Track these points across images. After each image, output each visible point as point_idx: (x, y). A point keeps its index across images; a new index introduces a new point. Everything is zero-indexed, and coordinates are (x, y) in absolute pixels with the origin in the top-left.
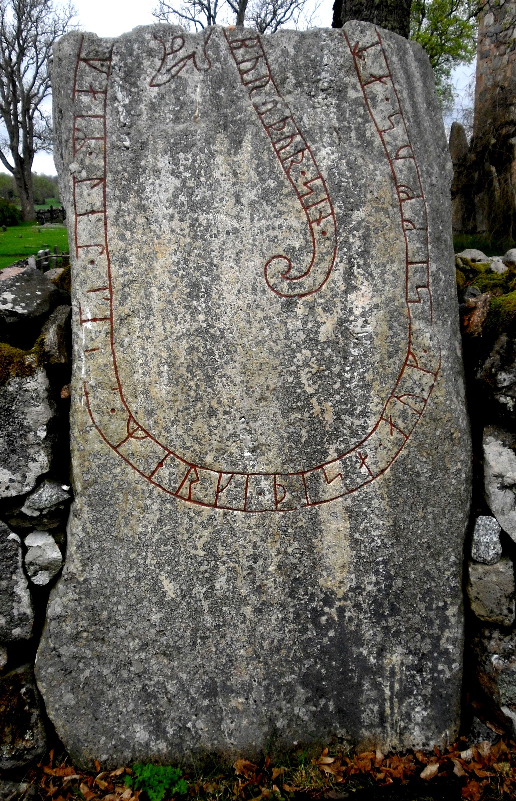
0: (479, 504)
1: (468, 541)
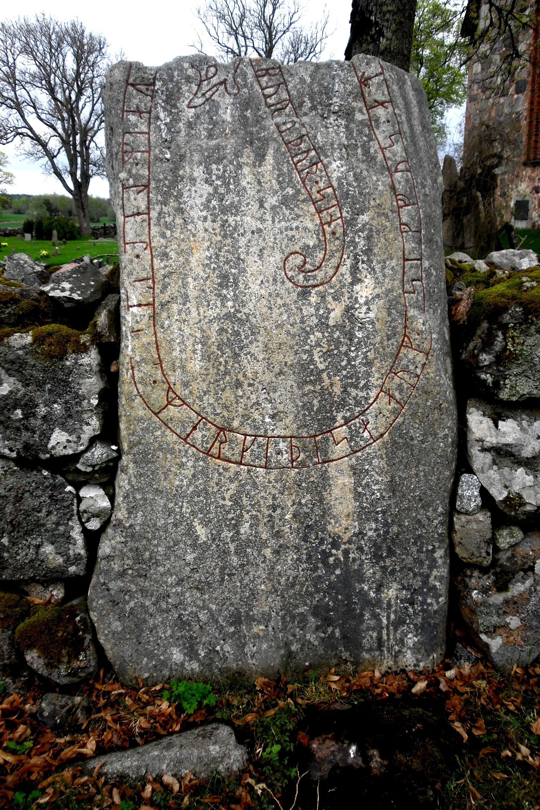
0: (463, 465)
1: (453, 495)
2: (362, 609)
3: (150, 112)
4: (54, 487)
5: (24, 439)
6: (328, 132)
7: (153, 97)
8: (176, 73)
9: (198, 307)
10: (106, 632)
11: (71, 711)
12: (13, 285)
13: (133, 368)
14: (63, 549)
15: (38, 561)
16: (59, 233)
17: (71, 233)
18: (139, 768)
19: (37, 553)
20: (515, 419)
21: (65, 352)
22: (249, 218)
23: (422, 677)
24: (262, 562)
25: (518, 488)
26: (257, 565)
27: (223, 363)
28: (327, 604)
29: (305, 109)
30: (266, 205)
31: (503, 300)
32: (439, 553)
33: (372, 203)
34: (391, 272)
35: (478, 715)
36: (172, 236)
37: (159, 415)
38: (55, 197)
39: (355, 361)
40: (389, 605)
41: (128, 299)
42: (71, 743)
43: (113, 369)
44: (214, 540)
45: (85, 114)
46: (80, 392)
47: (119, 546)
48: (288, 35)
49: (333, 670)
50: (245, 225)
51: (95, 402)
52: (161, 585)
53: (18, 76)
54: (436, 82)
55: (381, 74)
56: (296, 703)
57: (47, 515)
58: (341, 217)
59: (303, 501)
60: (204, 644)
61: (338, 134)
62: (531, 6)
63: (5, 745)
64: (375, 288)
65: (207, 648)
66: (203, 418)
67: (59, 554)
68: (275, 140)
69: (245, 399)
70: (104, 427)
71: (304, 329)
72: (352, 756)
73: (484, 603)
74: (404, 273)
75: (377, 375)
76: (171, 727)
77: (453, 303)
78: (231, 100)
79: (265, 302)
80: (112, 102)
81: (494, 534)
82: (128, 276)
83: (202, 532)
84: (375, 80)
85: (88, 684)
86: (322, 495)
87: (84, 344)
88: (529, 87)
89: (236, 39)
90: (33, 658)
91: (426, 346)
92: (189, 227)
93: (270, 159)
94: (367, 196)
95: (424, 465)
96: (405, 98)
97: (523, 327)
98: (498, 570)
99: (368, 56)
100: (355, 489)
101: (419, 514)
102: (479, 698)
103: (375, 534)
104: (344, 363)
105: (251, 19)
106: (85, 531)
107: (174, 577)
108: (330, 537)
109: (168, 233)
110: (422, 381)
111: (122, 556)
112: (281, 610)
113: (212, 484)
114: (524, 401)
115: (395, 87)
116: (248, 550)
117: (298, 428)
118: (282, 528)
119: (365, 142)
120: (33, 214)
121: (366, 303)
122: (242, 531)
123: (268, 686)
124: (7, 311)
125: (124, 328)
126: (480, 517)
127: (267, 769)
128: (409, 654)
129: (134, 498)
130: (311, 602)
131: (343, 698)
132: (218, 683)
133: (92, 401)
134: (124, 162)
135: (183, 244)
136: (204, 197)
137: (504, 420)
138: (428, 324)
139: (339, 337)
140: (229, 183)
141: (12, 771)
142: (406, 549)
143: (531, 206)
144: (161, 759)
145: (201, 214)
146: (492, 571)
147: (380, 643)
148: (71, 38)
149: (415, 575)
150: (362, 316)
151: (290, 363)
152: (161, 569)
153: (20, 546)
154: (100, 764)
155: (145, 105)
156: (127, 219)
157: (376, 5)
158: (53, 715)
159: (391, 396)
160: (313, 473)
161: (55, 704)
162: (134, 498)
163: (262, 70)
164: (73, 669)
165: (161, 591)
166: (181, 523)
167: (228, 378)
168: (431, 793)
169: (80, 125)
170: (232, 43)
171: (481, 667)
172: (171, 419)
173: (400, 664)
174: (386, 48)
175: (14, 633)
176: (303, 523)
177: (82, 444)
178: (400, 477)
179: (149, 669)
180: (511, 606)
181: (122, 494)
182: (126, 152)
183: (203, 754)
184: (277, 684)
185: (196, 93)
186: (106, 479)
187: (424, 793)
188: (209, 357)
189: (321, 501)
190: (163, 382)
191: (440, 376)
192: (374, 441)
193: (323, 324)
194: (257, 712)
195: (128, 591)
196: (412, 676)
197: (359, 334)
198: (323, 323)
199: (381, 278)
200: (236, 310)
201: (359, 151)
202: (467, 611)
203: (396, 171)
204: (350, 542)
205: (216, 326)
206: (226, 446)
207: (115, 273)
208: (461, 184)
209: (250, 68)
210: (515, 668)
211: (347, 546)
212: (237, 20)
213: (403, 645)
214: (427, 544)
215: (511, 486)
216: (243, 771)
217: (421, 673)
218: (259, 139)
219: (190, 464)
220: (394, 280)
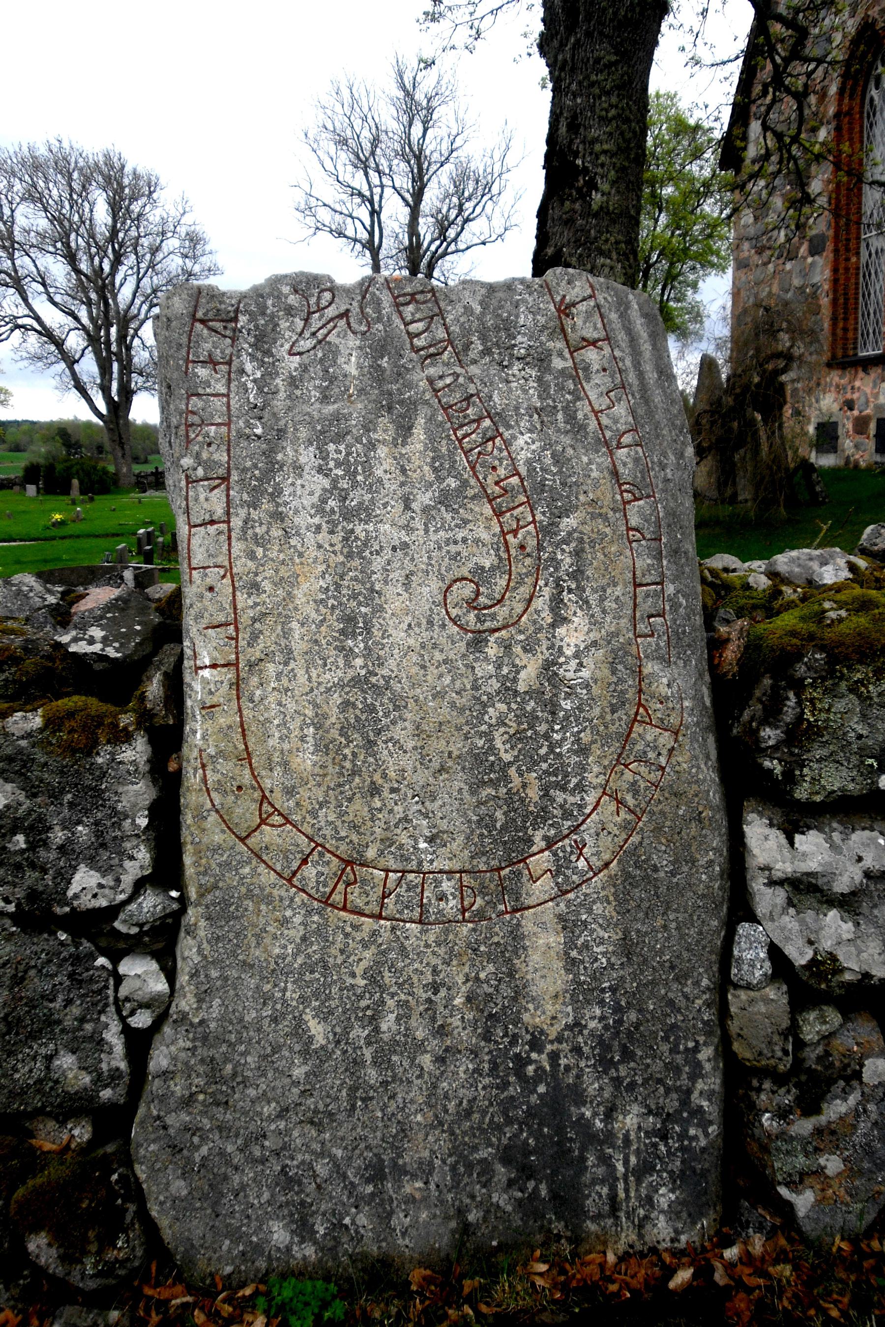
0: (740, 908)
1: (726, 957)
3: (229, 363)
4: (76, 959)
6: (510, 390)
7: (234, 339)
8: (270, 302)
9: (308, 668)
10: (162, 1198)
12: (13, 632)
13: (203, 766)
14: (90, 1061)
15: (49, 1081)
16: (81, 483)
19: (48, 1068)
20: (820, 830)
21: (96, 743)
22: (387, 526)
23: (685, 1260)
24: (418, 1077)
25: (829, 943)
26: (409, 1082)
27: (350, 757)
28: (525, 1142)
29: (473, 354)
30: (414, 506)
32: (706, 1054)
33: (582, 498)
34: (614, 606)
36: (265, 556)
37: (248, 841)
38: (75, 424)
39: (560, 747)
40: (627, 1141)
43: (172, 766)
44: (338, 1042)
45: (125, 294)
46: (120, 807)
47: (183, 1055)
49: (538, 1253)
50: (382, 538)
51: (143, 822)
52: (252, 1119)
53: (18, 236)
55: (590, 297)
57: (65, 1007)
58: (534, 521)
59: (482, 975)
60: (324, 1214)
61: (525, 392)
62: (828, 123)
65: (328, 1220)
66: (318, 845)
67: (85, 1069)
68: (427, 403)
69: (385, 812)
70: (156, 862)
71: (479, 699)
73: (782, 1135)
75: (596, 769)
77: (715, 645)
78: (358, 343)
79: (415, 658)
80: (170, 348)
82: (196, 619)
83: (318, 1030)
84: (582, 307)
86: (513, 965)
87: (125, 728)
88: (830, 246)
89: (366, 174)
91: (674, 720)
92: (293, 542)
93: (419, 433)
94: (574, 488)
95: (676, 911)
98: (803, 1078)
99: (570, 270)
100: (566, 953)
101: (670, 990)
102: (780, 1299)
103: (600, 1026)
104: (543, 751)
106: (127, 1031)
107: (273, 1105)
108: (527, 1032)
109: (260, 552)
110: (670, 775)
111: (188, 1071)
112: (450, 1155)
113: (334, 951)
114: (835, 800)
115: (614, 316)
116: (395, 1058)
117: (472, 857)
118: (449, 1020)
119: (568, 402)
120: (39, 452)
121: (576, 655)
122: (384, 1027)
125: (189, 703)
126: (771, 993)
128: (662, 1222)
130: (499, 1140)
131: (555, 1302)
132: (349, 1279)
133: (138, 821)
134: (189, 442)
135: (283, 569)
136: (317, 495)
137: (803, 833)
138: (676, 685)
139: (534, 710)
140: (355, 473)
142: (651, 1047)
143: (840, 431)
146: (795, 1080)
149: (668, 1091)
151: (456, 753)
152: (252, 1092)
153: (20, 1056)
155: (222, 352)
157: (583, 142)
159: (620, 802)
160: (497, 929)
163: (404, 295)
164: (106, 1263)
165: (252, 1127)
166: (283, 1015)
167: (357, 780)
169: (118, 312)
170: (359, 181)
171: (783, 1242)
172: (267, 848)
173: (647, 1238)
174: (601, 208)
176: (482, 1011)
178: (638, 931)
179: (233, 1260)
180: (827, 1138)
181: (187, 969)
182: (192, 425)
185: (302, 332)
186: (160, 945)
188: (326, 747)
189: (511, 974)
190: (253, 788)
191: (699, 768)
192: (595, 874)
193: (508, 690)
195: (198, 1129)
197: (567, 705)
198: (508, 689)
199: (599, 616)
201: (560, 416)
202: (755, 1147)
203: (618, 447)
204: (559, 1039)
205: (337, 698)
206: (356, 889)
208: (729, 401)
209: (386, 291)
210: (838, 1239)
211: (555, 1046)
212: (367, 146)
213: (652, 1206)
214: (686, 1039)
215: (819, 941)
217: (682, 1253)
218: (401, 402)
219: (298, 919)
220: (620, 617)
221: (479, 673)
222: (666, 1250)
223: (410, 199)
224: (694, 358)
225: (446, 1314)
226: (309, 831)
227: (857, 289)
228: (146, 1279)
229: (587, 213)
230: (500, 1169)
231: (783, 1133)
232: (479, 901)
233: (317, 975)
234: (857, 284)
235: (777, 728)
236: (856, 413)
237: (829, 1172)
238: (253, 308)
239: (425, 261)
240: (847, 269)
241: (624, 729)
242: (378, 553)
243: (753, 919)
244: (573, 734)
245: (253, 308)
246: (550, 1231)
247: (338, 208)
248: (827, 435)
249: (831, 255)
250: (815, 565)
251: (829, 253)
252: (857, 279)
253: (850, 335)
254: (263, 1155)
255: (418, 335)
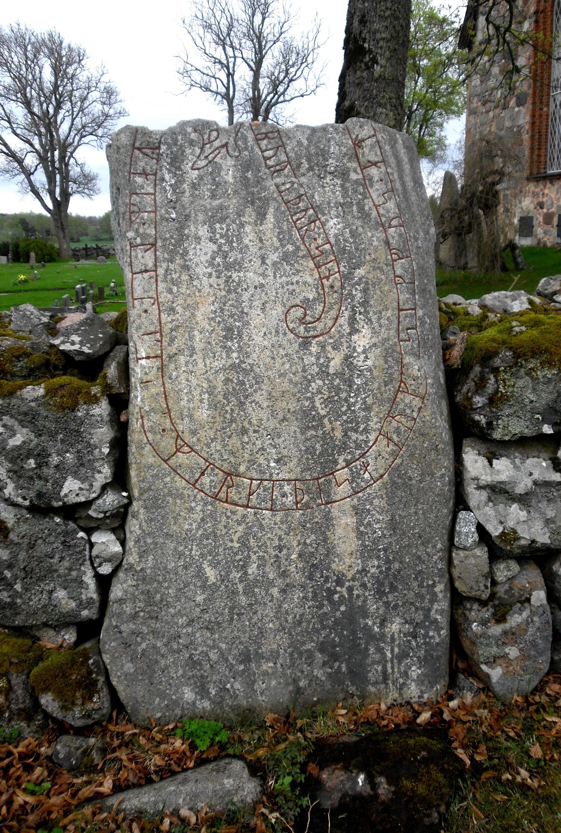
0: (460, 503)
1: (452, 532)
2: (367, 644)
3: (155, 174)
4: (66, 533)
5: (37, 487)
7: (158, 160)
8: (180, 138)
11: (86, 752)
13: (142, 417)
14: (75, 594)
15: (50, 606)
16: (37, 255)
17: (50, 255)
18: (156, 803)
19: (50, 598)
20: (508, 457)
21: (77, 404)
22: (251, 274)
23: (426, 708)
26: (265, 604)
29: (302, 170)
30: (268, 261)
31: (494, 345)
32: (440, 588)
33: (368, 257)
34: (386, 322)
35: (479, 742)
37: (169, 462)
38: (31, 216)
40: (393, 639)
41: (136, 352)
42: (88, 783)
43: (123, 418)
44: (223, 581)
45: (64, 129)
47: (131, 589)
48: (279, 44)
50: (248, 281)
51: (106, 451)
52: (172, 627)
54: (434, 92)
55: (373, 136)
56: (305, 738)
58: (339, 272)
59: (308, 541)
60: (215, 683)
61: (334, 193)
62: (530, 18)
63: (23, 787)
64: (372, 337)
66: (210, 464)
67: (72, 598)
68: (275, 199)
71: (306, 377)
72: (361, 784)
73: (483, 635)
74: (399, 322)
75: (375, 420)
76: (185, 764)
77: (447, 348)
78: (233, 163)
79: (268, 353)
81: (491, 567)
82: (137, 330)
83: (211, 574)
84: (369, 142)
85: (102, 726)
87: (95, 395)
88: (530, 100)
89: (224, 49)
90: (48, 701)
91: (422, 391)
93: (270, 218)
95: (423, 503)
96: (397, 157)
97: (514, 370)
101: (419, 550)
102: (481, 726)
103: (377, 571)
104: (344, 409)
105: (240, 29)
106: (98, 577)
107: (185, 618)
108: (334, 575)
109: (175, 289)
110: (419, 424)
111: (134, 598)
112: (289, 647)
113: (220, 527)
115: (387, 148)
116: (256, 590)
117: (302, 472)
118: (288, 568)
121: (364, 352)
122: (250, 571)
123: (277, 722)
124: (19, 365)
125: (133, 380)
127: (280, 800)
128: (413, 686)
129: (145, 542)
131: (351, 731)
132: (230, 720)
133: (103, 450)
134: (131, 222)
138: (424, 371)
139: (339, 384)
140: (232, 241)
141: (32, 810)
142: (407, 584)
143: (535, 222)
144: (177, 794)
145: (205, 270)
147: (385, 676)
148: (48, 48)
149: (417, 609)
150: (360, 364)
151: (292, 410)
152: (172, 611)
153: (33, 591)
154: (118, 801)
156: (135, 276)
157: (369, 32)
158: (68, 756)
159: (390, 439)
160: (317, 514)
161: (69, 746)
162: (145, 542)
163: (261, 134)
165: (172, 631)
167: (234, 425)
168: (436, 815)
169: (59, 141)
170: (219, 53)
171: (483, 697)
172: (180, 466)
173: (405, 696)
174: (380, 76)
175: (28, 677)
176: (308, 562)
177: (94, 492)
178: (400, 515)
179: (161, 709)
180: (510, 637)
181: (133, 539)
182: (133, 212)
183: (218, 787)
184: (287, 721)
186: (116, 525)
187: (429, 816)
188: (215, 405)
189: (325, 540)
190: (172, 430)
191: (436, 419)
192: (375, 482)
193: (323, 373)
194: (268, 746)
196: (416, 707)
197: (358, 381)
199: (377, 328)
200: (241, 361)
201: (355, 208)
203: (390, 227)
204: (353, 579)
205: (221, 377)
206: (233, 490)
207: (122, 322)
208: (463, 202)
211: (351, 583)
212: (225, 30)
213: (408, 677)
214: (428, 579)
216: (257, 803)
217: (425, 704)
218: (260, 199)
219: (199, 508)
221: (306, 362)
222: (416, 702)
223: (253, 66)
224: (440, 174)
225: (287, 738)
226: (205, 456)
227: (547, 129)
228: (110, 719)
229: (372, 79)
230: (319, 655)
231: (484, 633)
232: (306, 498)
233: (210, 541)
234: (547, 125)
235: (483, 396)
236: (545, 210)
237: (511, 657)
238: (169, 141)
239: (263, 108)
240: (541, 116)
241: (392, 396)
242: (246, 290)
243: (467, 508)
244: (362, 399)
245: (169, 141)
246: (348, 692)
247: (206, 72)
248: (526, 226)
249: (531, 107)
250: (509, 301)
251: (529, 105)
252: (547, 122)
253: (542, 159)
254: (179, 648)
255: (269, 158)
